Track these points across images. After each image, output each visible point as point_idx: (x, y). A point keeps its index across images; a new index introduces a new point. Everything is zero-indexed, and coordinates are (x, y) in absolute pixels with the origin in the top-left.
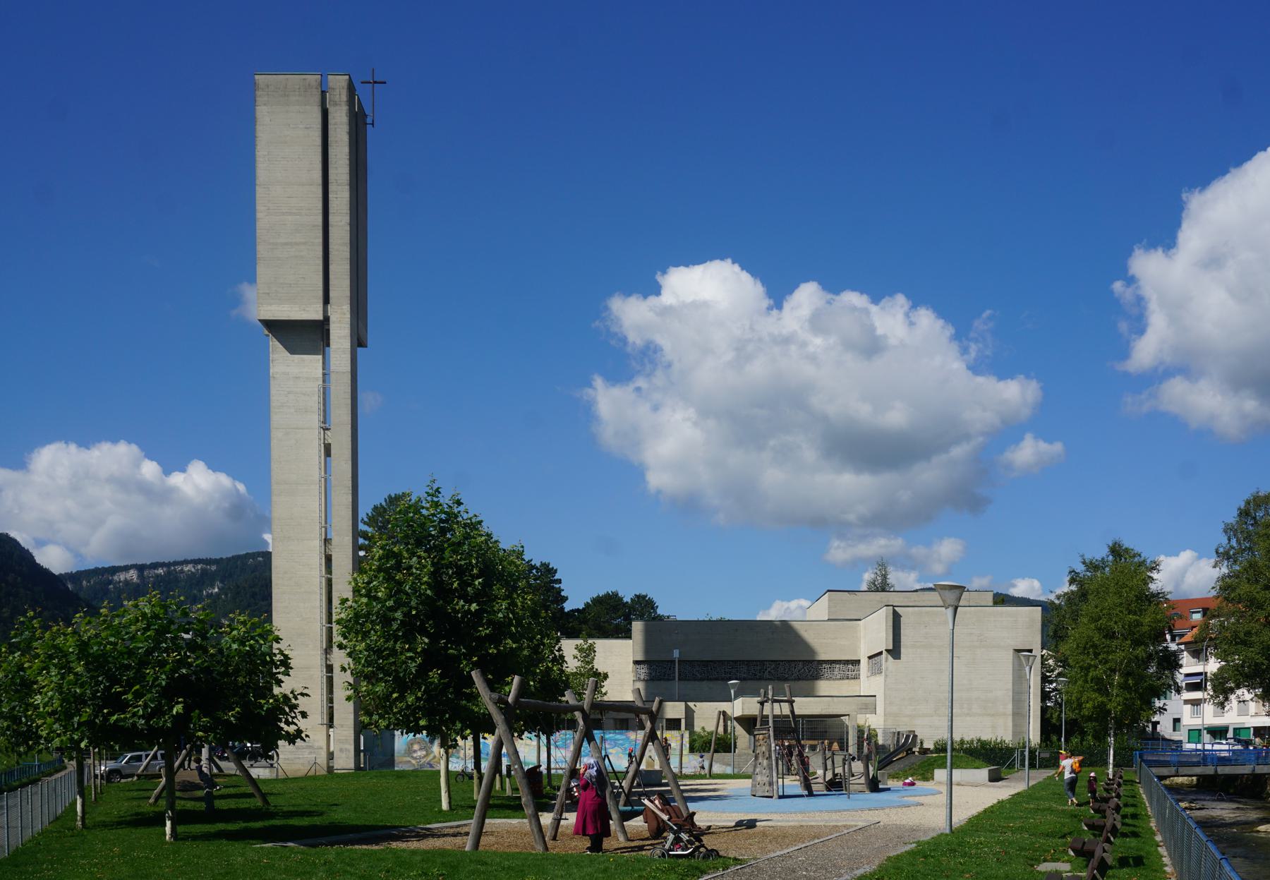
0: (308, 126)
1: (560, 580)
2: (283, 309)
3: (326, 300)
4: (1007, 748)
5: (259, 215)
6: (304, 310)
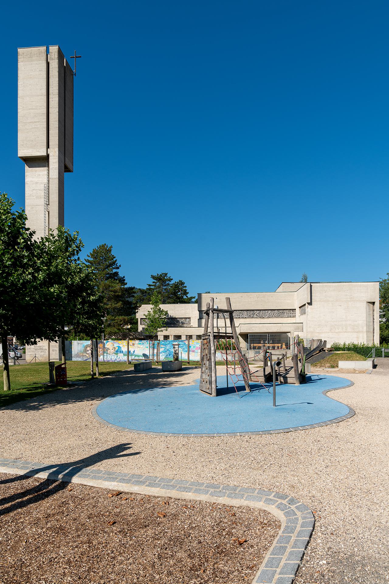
0: (41, 70)
1: (186, 286)
2: (30, 151)
3: (48, 147)
4: (368, 348)
5: (19, 111)
6: (38, 151)
